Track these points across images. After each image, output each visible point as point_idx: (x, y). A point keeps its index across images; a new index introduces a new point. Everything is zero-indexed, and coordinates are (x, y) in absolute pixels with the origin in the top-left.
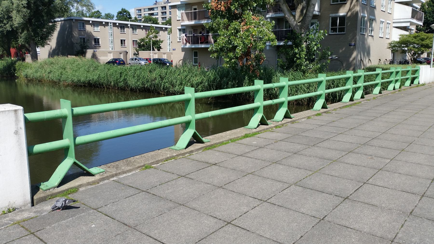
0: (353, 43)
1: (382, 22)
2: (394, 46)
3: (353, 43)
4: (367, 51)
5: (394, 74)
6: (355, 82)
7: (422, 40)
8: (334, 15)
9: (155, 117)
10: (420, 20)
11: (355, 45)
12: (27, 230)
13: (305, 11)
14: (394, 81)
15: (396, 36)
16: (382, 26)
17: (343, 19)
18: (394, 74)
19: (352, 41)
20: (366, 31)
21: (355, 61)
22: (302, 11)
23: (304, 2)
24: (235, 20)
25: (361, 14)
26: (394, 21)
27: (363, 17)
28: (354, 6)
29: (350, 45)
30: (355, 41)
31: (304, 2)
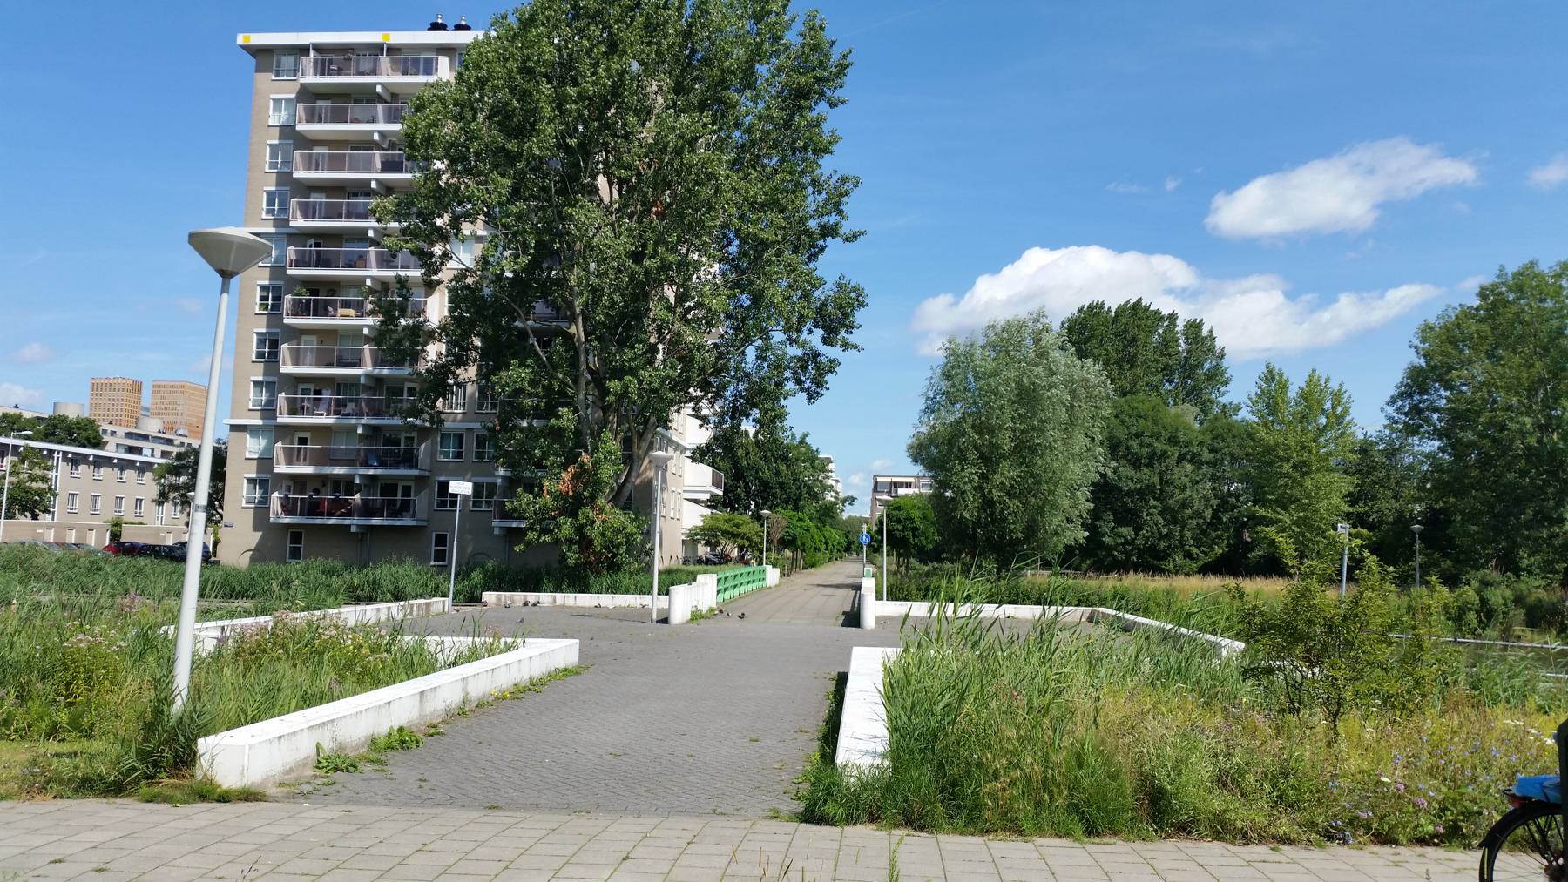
7: (737, 526)
15: (694, 517)
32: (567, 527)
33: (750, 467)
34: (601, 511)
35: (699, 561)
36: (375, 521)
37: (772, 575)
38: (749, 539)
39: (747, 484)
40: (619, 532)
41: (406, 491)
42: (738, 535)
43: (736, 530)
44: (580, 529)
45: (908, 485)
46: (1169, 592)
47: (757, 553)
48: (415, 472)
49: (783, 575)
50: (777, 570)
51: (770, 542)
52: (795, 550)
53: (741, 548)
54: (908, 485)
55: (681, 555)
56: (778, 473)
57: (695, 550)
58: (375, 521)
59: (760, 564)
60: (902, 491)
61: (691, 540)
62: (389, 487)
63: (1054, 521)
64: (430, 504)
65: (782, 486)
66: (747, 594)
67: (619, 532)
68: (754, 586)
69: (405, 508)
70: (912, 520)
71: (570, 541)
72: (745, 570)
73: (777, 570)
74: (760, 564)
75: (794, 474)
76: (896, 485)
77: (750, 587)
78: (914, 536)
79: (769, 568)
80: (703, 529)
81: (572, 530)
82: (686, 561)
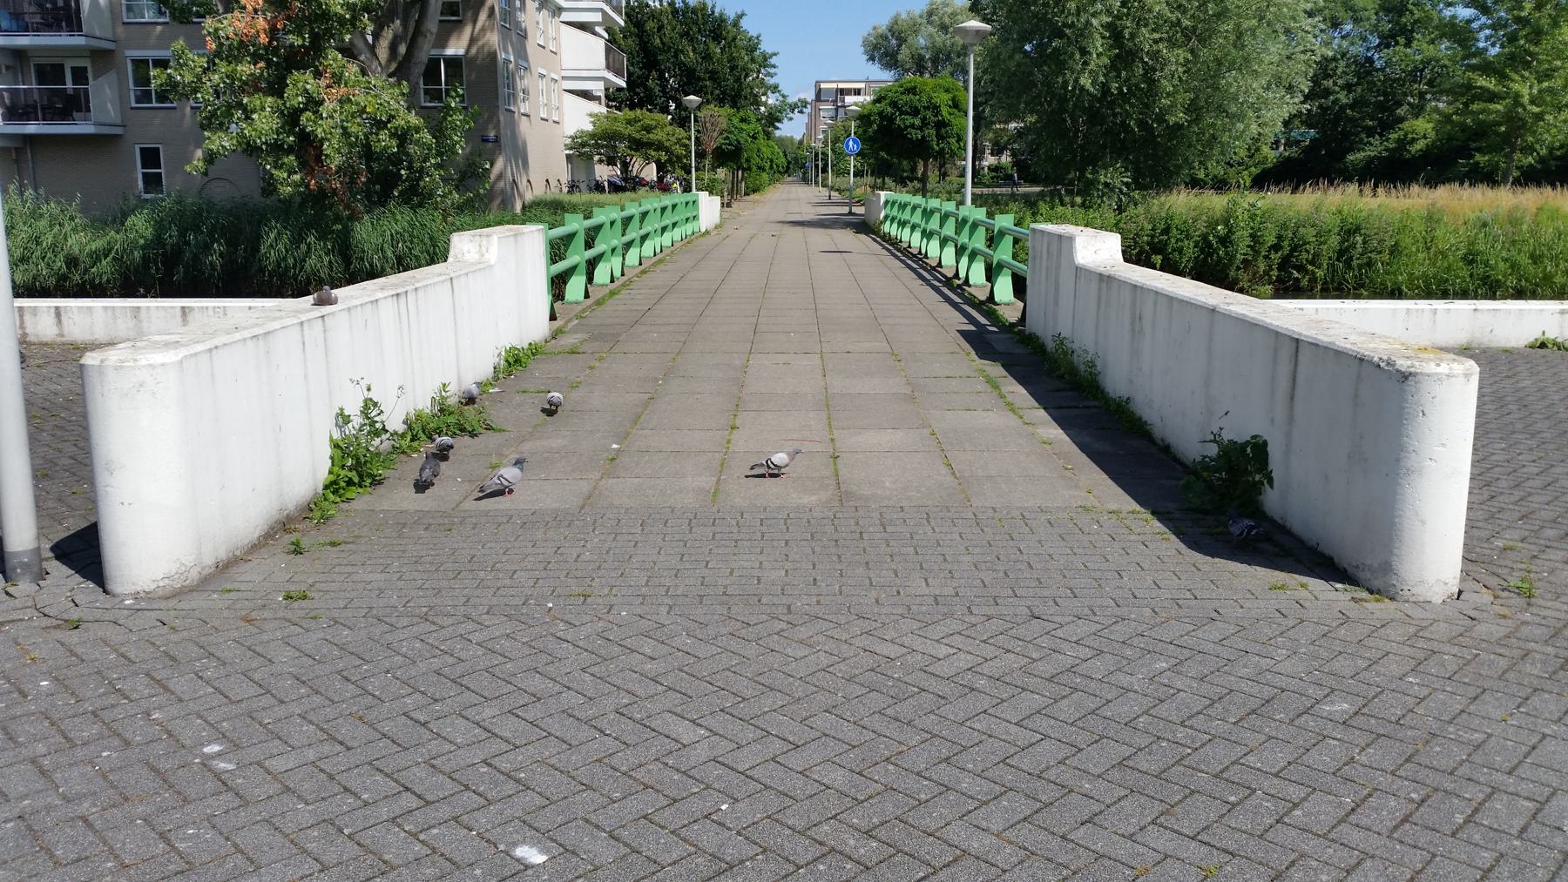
0: (492, 134)
1: (542, 76)
2: (583, 145)
3: (492, 134)
4: (520, 156)
5: (636, 220)
6: (589, 245)
7: (648, 129)
8: (434, 52)
9: (1119, 405)
10: (618, 73)
11: (497, 140)
12: (419, 797)
13: (402, 49)
14: (638, 242)
15: (579, 118)
16: (542, 84)
17: (453, 63)
18: (636, 220)
19: (486, 128)
20: (515, 103)
21: (501, 184)
22: (393, 48)
23: (398, 22)
24: (298, 69)
25: (501, 56)
26: (564, 73)
27: (507, 61)
28: (483, 29)
29: (486, 141)
30: (497, 126)
31: (398, 22)
32: (264, 122)
33: (665, 48)
34: (337, 79)
35: (599, 188)
36: (32, 128)
37: (709, 208)
38: (667, 150)
39: (661, 77)
40: (380, 125)
41: (80, 75)
42: (650, 145)
43: (644, 136)
44: (291, 118)
45: (857, 92)
46: (1432, 219)
47: (680, 172)
48: (78, 41)
49: (726, 205)
50: (717, 199)
51: (701, 155)
52: (738, 165)
53: (661, 167)
54: (857, 92)
55: (565, 178)
56: (707, 57)
57: (591, 171)
58: (32, 128)
59: (687, 189)
60: (849, 99)
61: (582, 151)
62: (50, 72)
63: (1245, 86)
64: (123, 98)
65: (713, 76)
66: (660, 257)
67: (380, 125)
68: (677, 234)
69: (73, 105)
70: (936, 109)
71: (277, 148)
72: (667, 200)
73: (717, 199)
74: (687, 189)
75: (732, 59)
76: (843, 92)
77: (666, 239)
78: (940, 137)
79: (703, 196)
80: (593, 135)
81: (276, 123)
82: (573, 187)
